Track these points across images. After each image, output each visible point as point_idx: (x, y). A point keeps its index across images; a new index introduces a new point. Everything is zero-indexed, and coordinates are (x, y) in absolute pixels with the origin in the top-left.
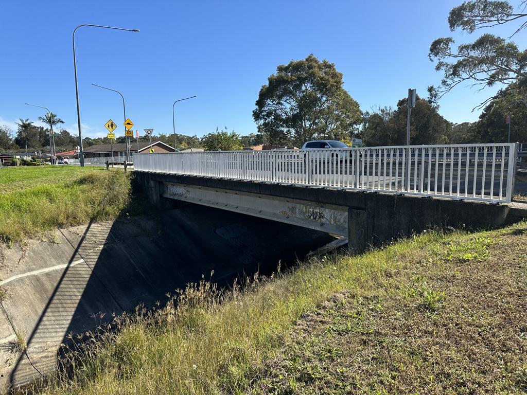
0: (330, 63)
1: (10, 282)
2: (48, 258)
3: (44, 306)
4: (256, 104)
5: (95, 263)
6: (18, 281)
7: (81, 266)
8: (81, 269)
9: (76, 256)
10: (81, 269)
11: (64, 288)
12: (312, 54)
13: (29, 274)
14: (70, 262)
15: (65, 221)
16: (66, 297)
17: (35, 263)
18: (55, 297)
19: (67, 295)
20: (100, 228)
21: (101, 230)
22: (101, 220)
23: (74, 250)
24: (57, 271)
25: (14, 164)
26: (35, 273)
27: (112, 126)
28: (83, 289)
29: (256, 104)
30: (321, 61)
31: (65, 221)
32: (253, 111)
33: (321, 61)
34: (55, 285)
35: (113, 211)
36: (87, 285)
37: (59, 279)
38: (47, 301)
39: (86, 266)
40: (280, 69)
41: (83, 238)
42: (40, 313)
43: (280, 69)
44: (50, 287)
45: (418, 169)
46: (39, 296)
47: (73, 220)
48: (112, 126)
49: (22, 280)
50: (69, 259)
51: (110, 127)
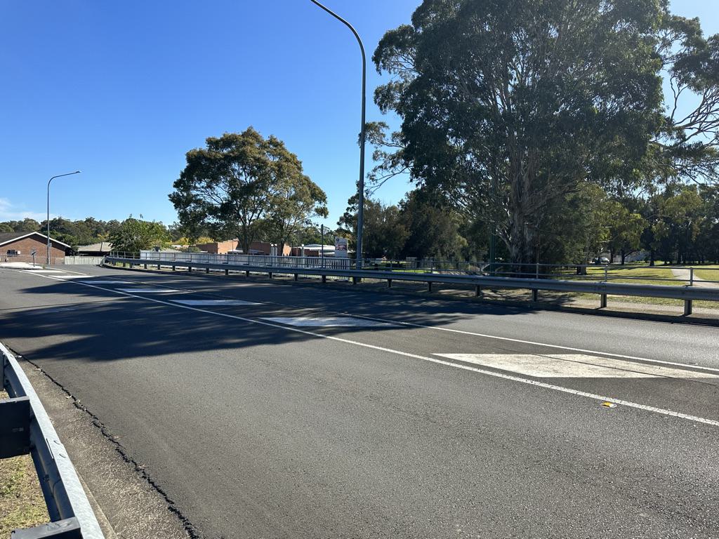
4: (174, 186)
29: (174, 186)
30: (266, 139)
33: (266, 139)
40: (212, 143)
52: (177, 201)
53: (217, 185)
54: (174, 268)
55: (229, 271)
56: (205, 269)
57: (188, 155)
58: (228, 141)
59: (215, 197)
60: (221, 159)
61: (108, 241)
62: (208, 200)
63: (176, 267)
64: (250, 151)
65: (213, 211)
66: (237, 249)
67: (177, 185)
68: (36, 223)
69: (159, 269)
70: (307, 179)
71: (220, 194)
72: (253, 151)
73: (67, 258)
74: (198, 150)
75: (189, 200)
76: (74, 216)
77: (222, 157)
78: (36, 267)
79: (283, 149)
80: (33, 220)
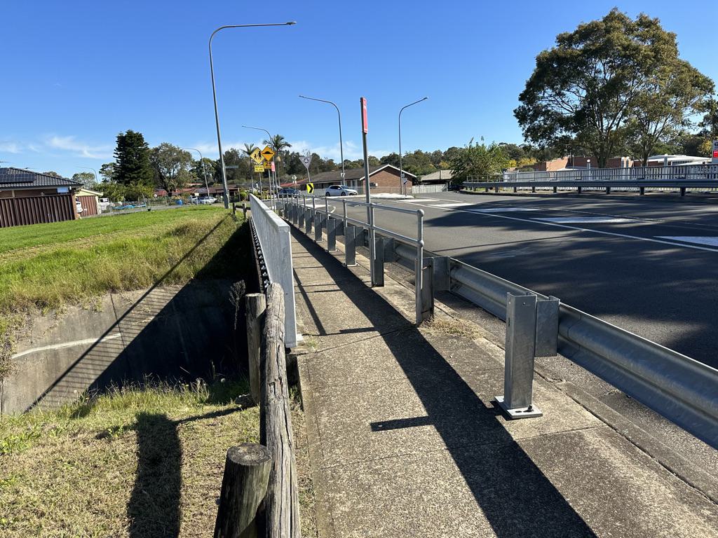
0: (651, 18)
1: (24, 356)
2: (80, 329)
3: (47, 387)
4: (520, 99)
5: (132, 339)
6: (32, 355)
7: (115, 342)
8: (112, 346)
9: (114, 329)
10: (112, 346)
11: (82, 368)
12: (616, 9)
13: (49, 347)
14: (103, 337)
15: (120, 285)
16: (76, 380)
17: (63, 335)
18: (64, 379)
19: (79, 378)
20: (162, 294)
21: (162, 297)
22: (169, 283)
23: (116, 321)
24: (82, 346)
25: (178, 203)
26: (56, 347)
27: (260, 156)
28: (102, 372)
29: (520, 99)
30: (633, 18)
31: (120, 285)
32: (515, 111)
33: (633, 18)
34: (72, 362)
35: (187, 271)
36: (110, 367)
37: (80, 356)
38: (53, 381)
39: (121, 342)
40: (561, 39)
41: (135, 306)
42: (39, 394)
43: (561, 39)
44: (65, 365)
45: (569, 212)
46: (47, 375)
47: (131, 283)
48: (260, 156)
49: (38, 354)
50: (104, 332)
51: (258, 157)
52: (521, 116)
53: (568, 90)
54: (642, 191)
55: (646, 189)
56: (552, 188)
57: (538, 59)
58: (585, 33)
59: (565, 106)
60: (579, 55)
61: (449, 169)
62: (557, 109)
63: (646, 189)
64: (618, 38)
65: (564, 122)
66: (566, 167)
67: (522, 97)
68: (377, 160)
69: (533, 192)
70: (686, 65)
71: (574, 98)
72: (620, 37)
73: (414, 187)
74: (550, 51)
75: (537, 113)
76: (406, 150)
77: (580, 53)
78: (408, 197)
79: (658, 28)
80: (374, 157)
